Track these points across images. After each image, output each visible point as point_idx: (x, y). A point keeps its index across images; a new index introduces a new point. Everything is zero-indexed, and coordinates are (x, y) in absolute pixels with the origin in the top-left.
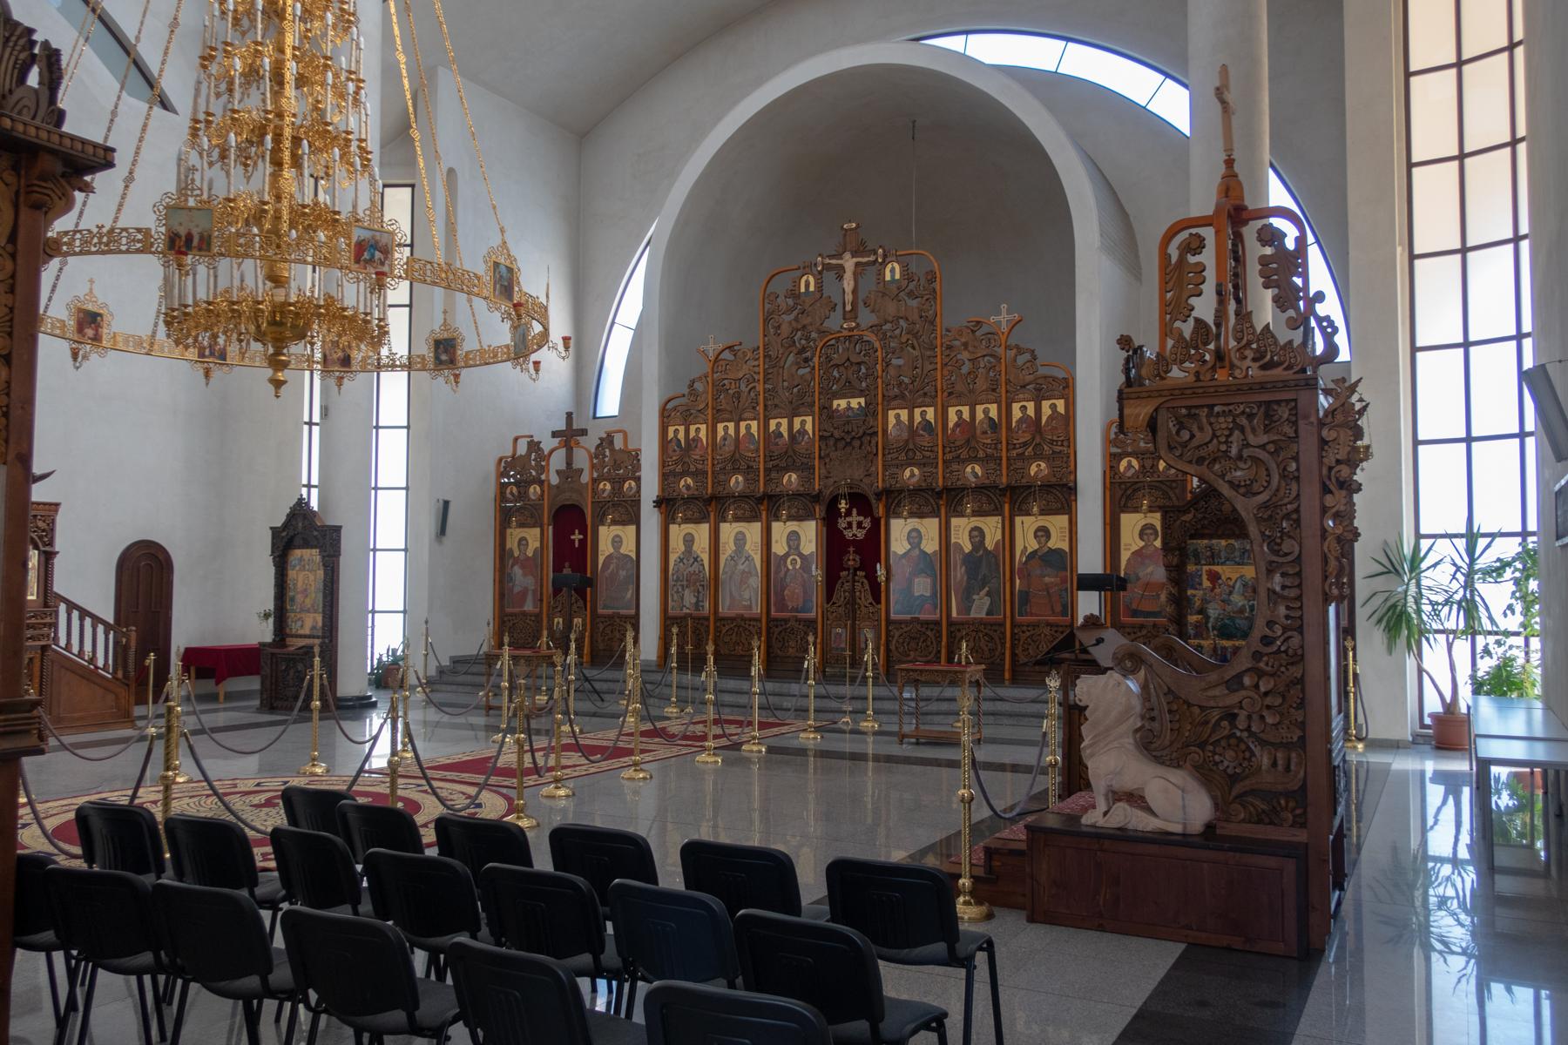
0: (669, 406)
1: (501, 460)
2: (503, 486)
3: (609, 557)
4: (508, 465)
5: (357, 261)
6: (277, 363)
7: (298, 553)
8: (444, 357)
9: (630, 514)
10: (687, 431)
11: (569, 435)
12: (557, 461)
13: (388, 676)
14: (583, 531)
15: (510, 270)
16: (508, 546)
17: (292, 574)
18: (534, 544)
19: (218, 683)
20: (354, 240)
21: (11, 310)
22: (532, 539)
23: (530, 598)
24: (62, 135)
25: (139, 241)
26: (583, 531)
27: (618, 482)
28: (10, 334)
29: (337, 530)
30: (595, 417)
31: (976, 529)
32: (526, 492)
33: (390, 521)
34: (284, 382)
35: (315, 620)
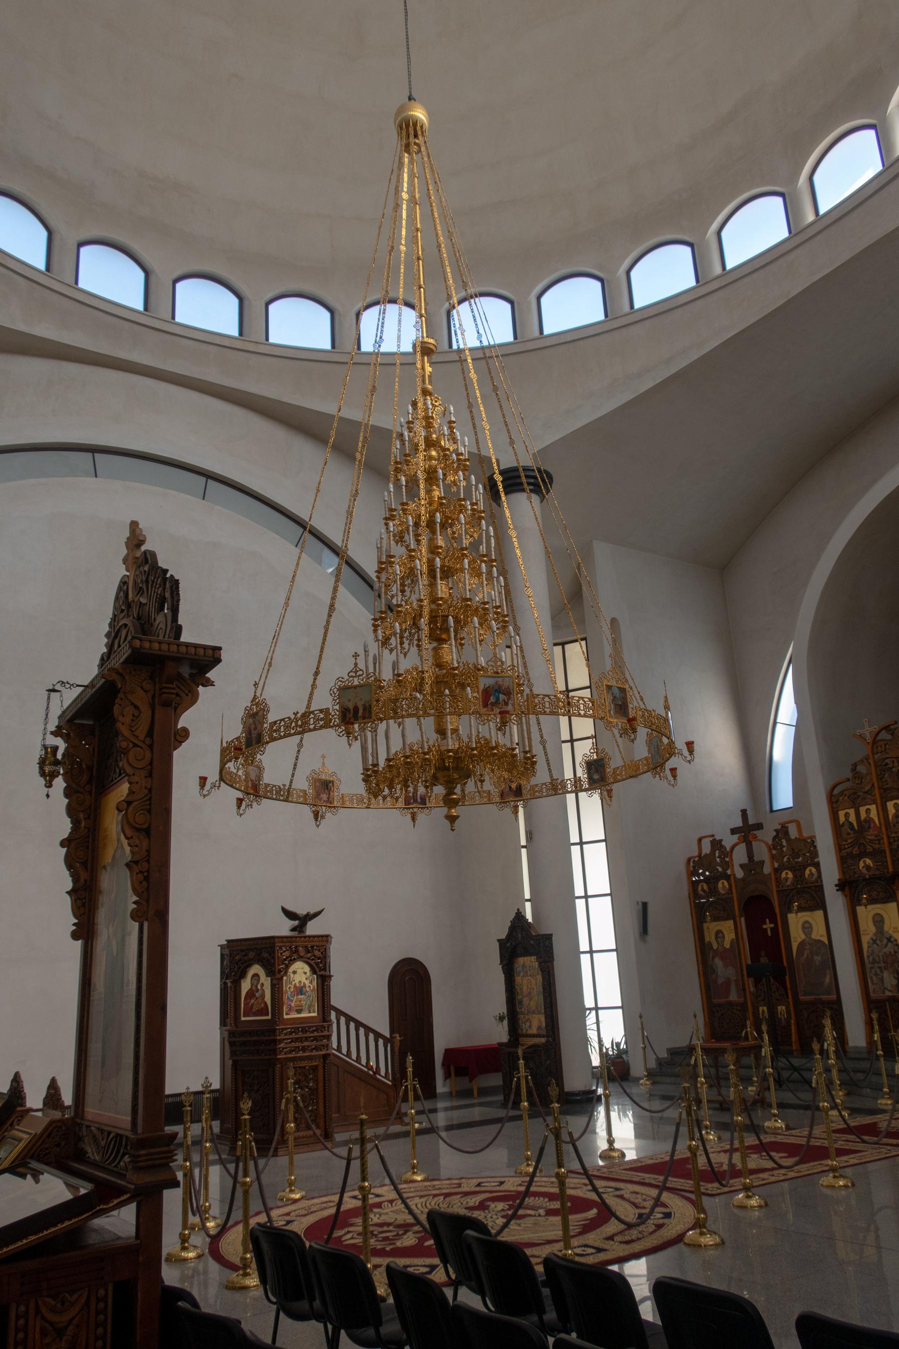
0: (836, 792)
1: (689, 860)
2: (694, 885)
3: (802, 944)
4: (696, 864)
5: (485, 705)
6: (449, 802)
7: (521, 960)
8: (596, 777)
9: (814, 899)
10: (858, 814)
11: (747, 830)
12: (740, 856)
13: (617, 1069)
14: (773, 920)
15: (623, 690)
16: (707, 939)
17: (518, 979)
18: (729, 937)
19: (471, 1081)
20: (481, 687)
21: (150, 790)
22: (726, 931)
23: (733, 987)
24: (179, 645)
25: (322, 719)
26: (773, 920)
27: (798, 870)
28: (149, 811)
29: (549, 937)
30: (772, 811)
31: (806, 922)
32: (716, 888)
33: (597, 926)
34: (457, 817)
35: (540, 1021)
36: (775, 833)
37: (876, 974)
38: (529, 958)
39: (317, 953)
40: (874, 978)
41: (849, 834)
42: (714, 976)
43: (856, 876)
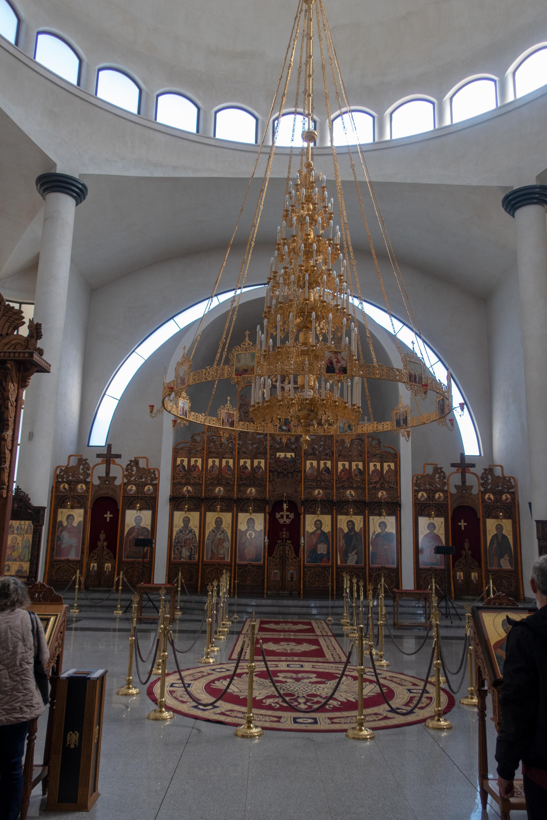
10: (189, 462)
12: (101, 471)
16: (59, 519)
27: (140, 486)
36: (483, 471)
37: (178, 549)
38: (18, 522)
39: (511, 511)
40: (176, 551)
41: (181, 471)
42: (59, 542)
43: (180, 495)
